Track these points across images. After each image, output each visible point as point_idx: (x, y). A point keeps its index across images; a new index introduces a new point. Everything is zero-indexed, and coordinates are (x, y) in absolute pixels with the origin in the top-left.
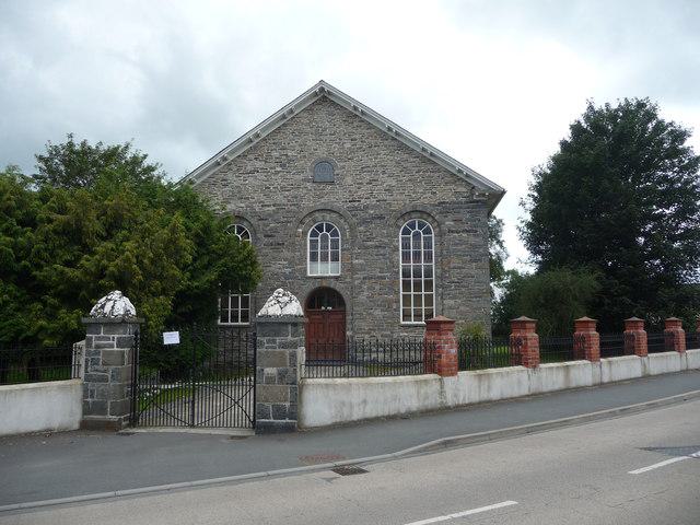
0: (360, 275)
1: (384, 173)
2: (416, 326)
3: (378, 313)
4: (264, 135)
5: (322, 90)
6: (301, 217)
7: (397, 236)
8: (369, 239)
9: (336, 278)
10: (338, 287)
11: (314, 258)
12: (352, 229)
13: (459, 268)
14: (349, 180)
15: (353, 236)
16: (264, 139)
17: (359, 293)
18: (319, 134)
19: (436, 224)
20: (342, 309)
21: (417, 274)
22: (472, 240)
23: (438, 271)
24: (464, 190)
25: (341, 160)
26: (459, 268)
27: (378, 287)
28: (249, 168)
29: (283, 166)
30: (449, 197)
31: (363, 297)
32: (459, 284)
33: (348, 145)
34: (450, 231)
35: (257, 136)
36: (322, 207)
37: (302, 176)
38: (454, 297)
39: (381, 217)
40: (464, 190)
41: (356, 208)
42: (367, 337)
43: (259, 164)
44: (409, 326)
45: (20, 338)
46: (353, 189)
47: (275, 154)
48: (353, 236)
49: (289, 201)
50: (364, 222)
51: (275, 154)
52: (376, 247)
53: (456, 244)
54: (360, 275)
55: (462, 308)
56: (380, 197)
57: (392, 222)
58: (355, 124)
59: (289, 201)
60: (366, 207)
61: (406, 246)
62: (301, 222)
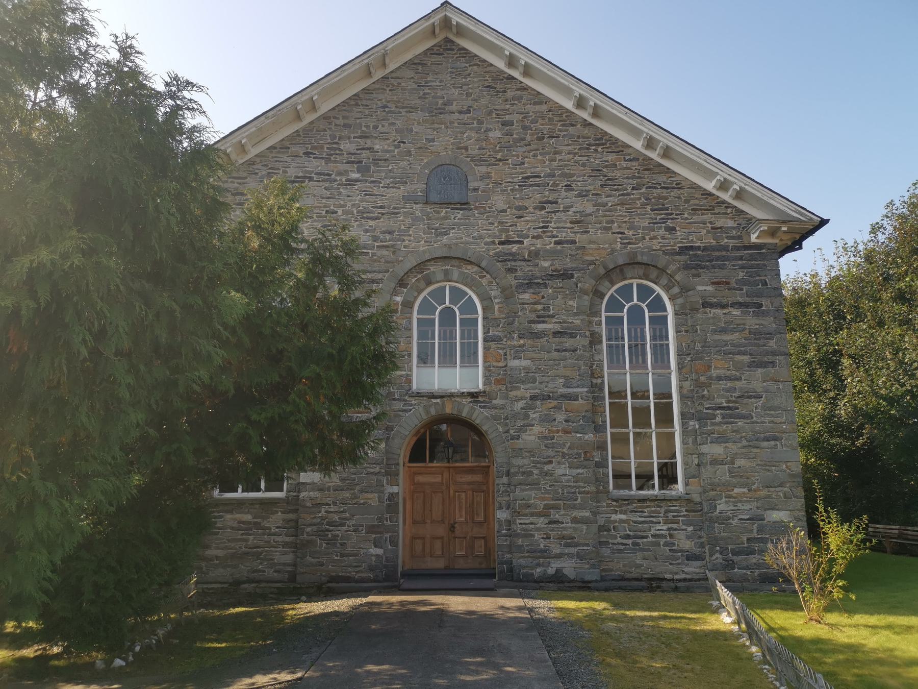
0: (524, 391)
1: (569, 187)
2: (643, 500)
3: (562, 470)
4: (324, 108)
5: (446, 23)
6: (400, 270)
7: (598, 314)
8: (541, 319)
9: (473, 395)
10: (479, 416)
11: (425, 359)
12: (507, 295)
13: (728, 378)
14: (499, 201)
15: (511, 316)
16: (325, 117)
17: (522, 429)
18: (437, 111)
19: (676, 290)
20: (667, 342)
21: (639, 394)
22: (752, 322)
23: (687, 384)
24: (730, 223)
25: (481, 161)
26: (728, 378)
27: (560, 417)
28: (292, 172)
29: (364, 170)
30: (702, 238)
31: (530, 438)
32: (731, 413)
33: (495, 134)
34: (706, 304)
35: (313, 106)
36: (445, 252)
37: (402, 190)
38: (722, 439)
39: (566, 275)
40: (730, 223)
41: (513, 257)
42: (541, 522)
43: (314, 165)
44: (629, 500)
45: (634, 657)
46: (508, 218)
47: (346, 146)
48: (511, 316)
49: (375, 239)
50: (530, 284)
51: (346, 146)
52: (556, 334)
53: (723, 331)
54: (524, 391)
55: (739, 462)
56: (562, 236)
57: (588, 284)
58: (510, 94)
59: (375, 239)
60: (535, 255)
61: (615, 336)
62: (402, 283)
